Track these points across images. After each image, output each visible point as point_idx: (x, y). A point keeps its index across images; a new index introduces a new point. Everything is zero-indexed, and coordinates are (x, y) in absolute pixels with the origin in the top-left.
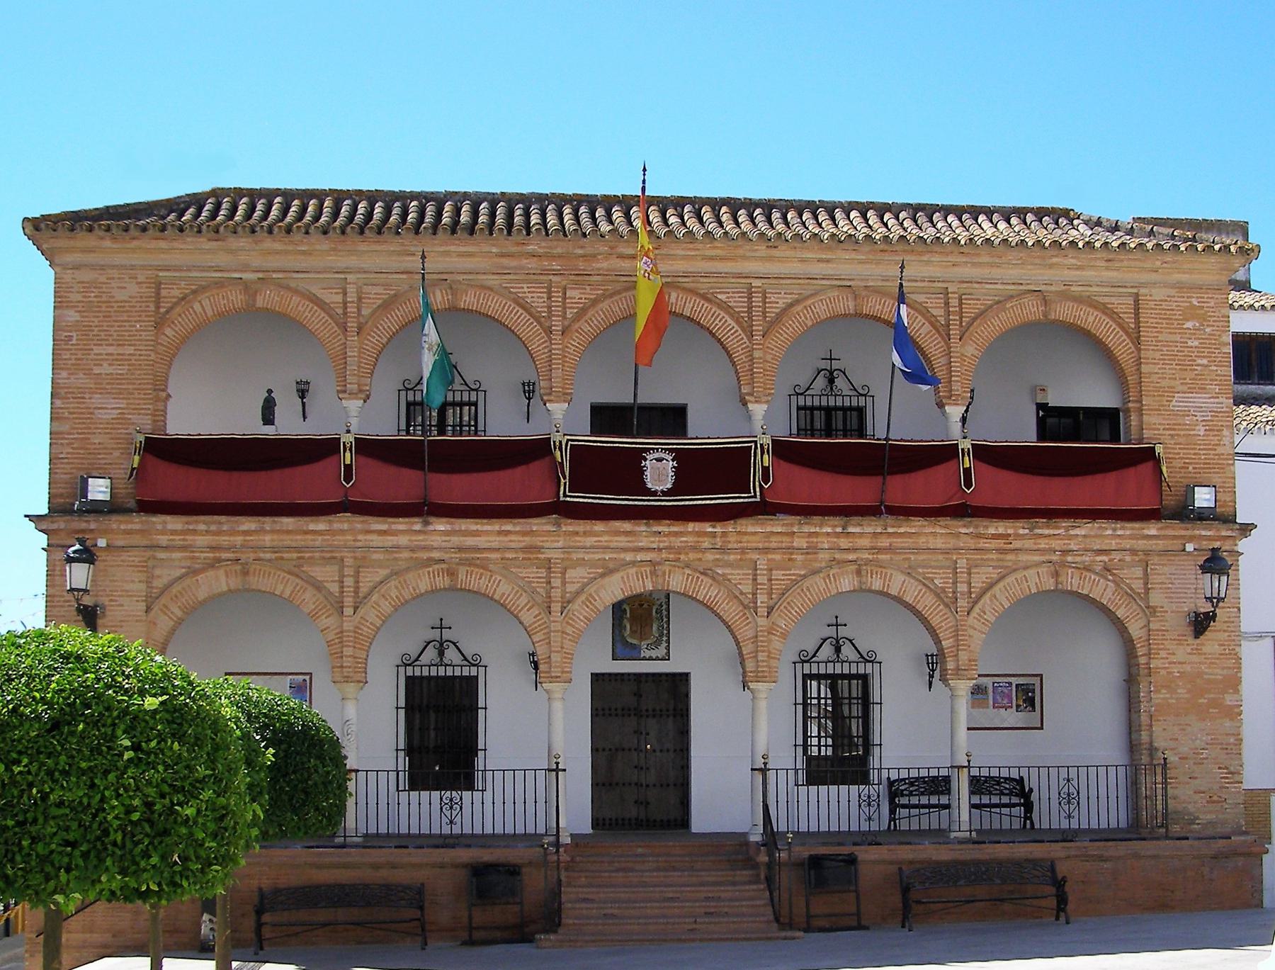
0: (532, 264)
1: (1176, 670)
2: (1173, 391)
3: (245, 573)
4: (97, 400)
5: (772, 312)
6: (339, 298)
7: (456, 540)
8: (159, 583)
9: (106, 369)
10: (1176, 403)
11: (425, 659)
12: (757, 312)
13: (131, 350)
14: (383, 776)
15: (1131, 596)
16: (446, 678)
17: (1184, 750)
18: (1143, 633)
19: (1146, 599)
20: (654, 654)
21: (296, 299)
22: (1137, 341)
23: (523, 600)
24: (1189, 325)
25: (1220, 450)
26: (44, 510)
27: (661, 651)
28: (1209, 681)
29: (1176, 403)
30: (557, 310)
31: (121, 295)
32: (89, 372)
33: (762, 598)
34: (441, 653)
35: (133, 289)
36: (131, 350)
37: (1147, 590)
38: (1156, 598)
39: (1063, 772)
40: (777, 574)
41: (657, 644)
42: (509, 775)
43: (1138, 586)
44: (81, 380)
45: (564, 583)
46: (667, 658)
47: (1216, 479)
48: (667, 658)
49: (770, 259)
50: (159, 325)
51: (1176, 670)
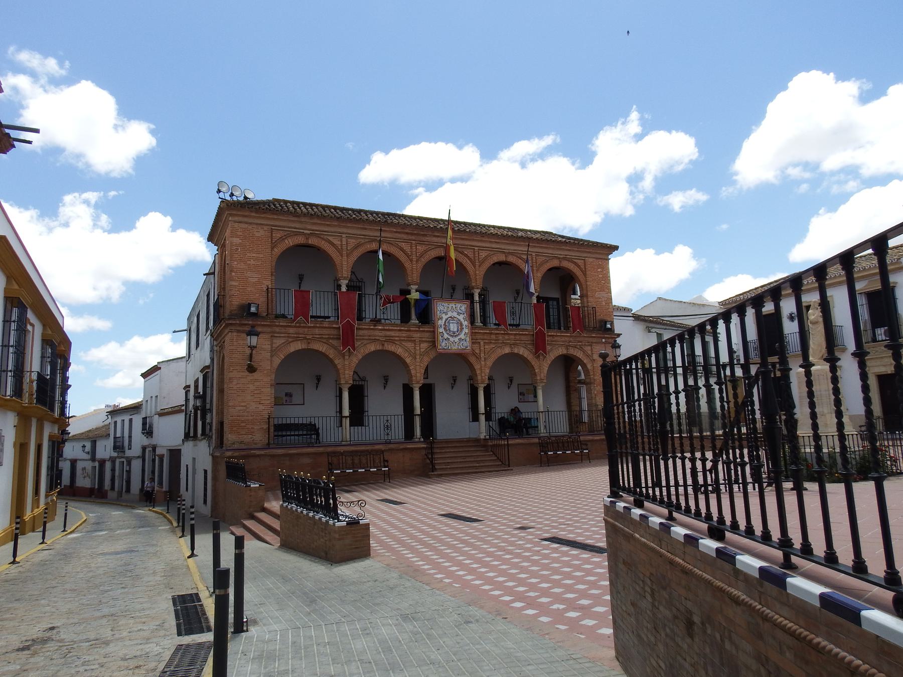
0: (405, 236)
4: (249, 274)
9: (252, 262)
10: (597, 295)
15: (588, 356)
29: (597, 295)
31: (257, 234)
33: (482, 355)
40: (486, 347)
43: (589, 352)
49: (481, 241)
50: (272, 249)
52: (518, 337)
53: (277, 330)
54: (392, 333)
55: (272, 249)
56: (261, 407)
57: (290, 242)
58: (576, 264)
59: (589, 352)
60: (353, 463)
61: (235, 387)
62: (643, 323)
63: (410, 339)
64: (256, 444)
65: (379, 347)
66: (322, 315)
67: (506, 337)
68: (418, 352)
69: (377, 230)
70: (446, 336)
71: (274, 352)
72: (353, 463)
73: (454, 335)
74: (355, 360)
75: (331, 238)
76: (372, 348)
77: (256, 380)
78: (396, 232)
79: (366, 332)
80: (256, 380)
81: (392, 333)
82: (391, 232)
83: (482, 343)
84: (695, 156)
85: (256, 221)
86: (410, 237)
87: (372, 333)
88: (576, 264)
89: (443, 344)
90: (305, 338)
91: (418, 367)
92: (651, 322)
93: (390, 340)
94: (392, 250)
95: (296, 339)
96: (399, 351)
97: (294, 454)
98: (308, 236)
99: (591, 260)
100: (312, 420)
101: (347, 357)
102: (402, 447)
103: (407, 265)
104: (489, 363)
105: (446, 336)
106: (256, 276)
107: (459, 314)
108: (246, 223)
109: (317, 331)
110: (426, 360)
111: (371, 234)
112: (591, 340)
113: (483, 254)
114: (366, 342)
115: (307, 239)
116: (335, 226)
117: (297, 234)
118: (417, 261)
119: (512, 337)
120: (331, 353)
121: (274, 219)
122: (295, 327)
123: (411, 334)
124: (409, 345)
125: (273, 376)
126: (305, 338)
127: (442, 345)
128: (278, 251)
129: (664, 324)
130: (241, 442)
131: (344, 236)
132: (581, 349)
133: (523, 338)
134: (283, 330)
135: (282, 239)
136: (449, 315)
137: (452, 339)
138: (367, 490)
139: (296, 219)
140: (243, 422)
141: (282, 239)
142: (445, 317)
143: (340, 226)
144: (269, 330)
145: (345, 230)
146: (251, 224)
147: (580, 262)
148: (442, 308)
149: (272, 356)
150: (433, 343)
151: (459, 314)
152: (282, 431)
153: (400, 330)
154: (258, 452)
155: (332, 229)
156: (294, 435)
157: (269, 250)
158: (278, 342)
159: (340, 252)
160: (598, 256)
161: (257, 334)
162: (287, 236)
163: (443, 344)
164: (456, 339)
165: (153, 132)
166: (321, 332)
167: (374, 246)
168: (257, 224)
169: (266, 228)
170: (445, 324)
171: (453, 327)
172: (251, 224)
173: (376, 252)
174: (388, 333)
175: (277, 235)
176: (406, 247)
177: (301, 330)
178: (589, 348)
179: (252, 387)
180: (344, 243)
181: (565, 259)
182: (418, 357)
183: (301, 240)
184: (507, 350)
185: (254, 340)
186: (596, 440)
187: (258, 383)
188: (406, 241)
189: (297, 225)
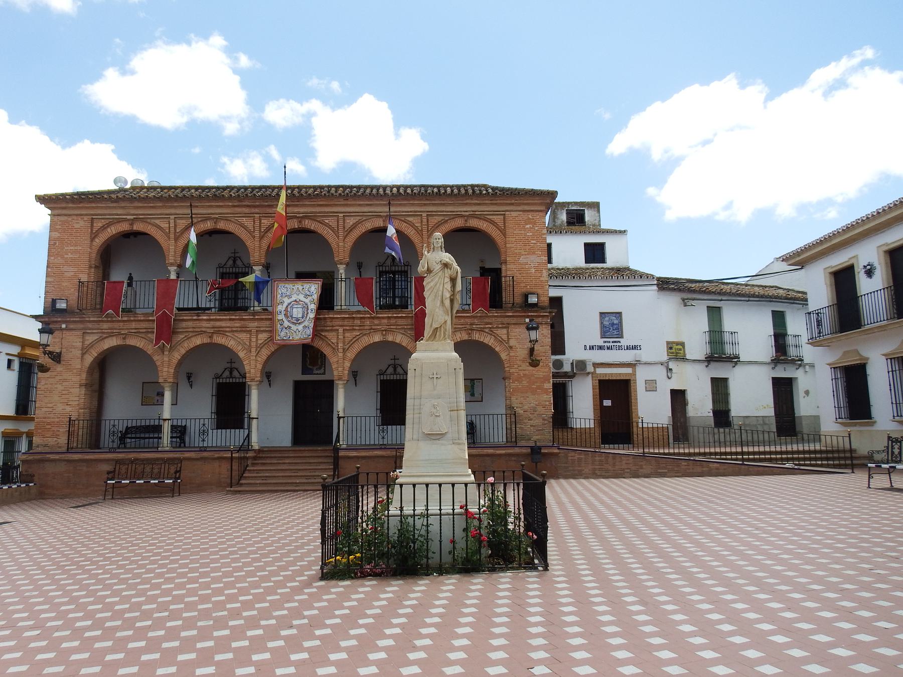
0: (247, 210)
1: (521, 373)
2: (520, 254)
3: (124, 339)
4: (66, 268)
5: (348, 226)
6: (167, 225)
7: (212, 324)
8: (87, 343)
9: (70, 255)
10: (522, 260)
11: (225, 375)
12: (341, 227)
13: (80, 248)
14: (500, 416)
15: (501, 342)
16: (236, 383)
17: (526, 407)
18: (507, 358)
19: (508, 343)
20: (318, 372)
21: (150, 226)
22: (505, 235)
23: (240, 348)
24: (528, 226)
25: (542, 279)
26: (40, 312)
27: (322, 371)
28: (537, 378)
29: (522, 260)
30: (257, 229)
31: (77, 226)
32: (63, 258)
33: (340, 345)
34: (231, 373)
35: (82, 223)
36: (80, 248)
37: (508, 339)
38: (512, 342)
39: (112, 422)
40: (347, 335)
41: (320, 368)
42: (354, 419)
43: (505, 337)
44: (59, 260)
45: (257, 340)
46: (324, 374)
47: (540, 291)
48: (324, 374)
49: (346, 205)
50: (92, 240)
51: (521, 373)
52: (393, 321)
53: (90, 325)
54: (223, 324)
55: (92, 240)
56: (68, 409)
57: (113, 230)
58: (492, 222)
59: (505, 337)
60: (152, 472)
61: (43, 388)
62: (674, 293)
63: (244, 330)
64: (60, 447)
65: (206, 340)
66: (186, 306)
67: (376, 322)
68: (253, 344)
69: (384, 205)
70: (286, 324)
71: (85, 351)
72: (152, 472)
73: (297, 322)
74: (177, 356)
75: (157, 222)
76: (198, 341)
77: (65, 380)
78: (235, 206)
79: (190, 324)
80: (65, 380)
81: (223, 324)
82: (228, 206)
83: (341, 330)
84: (218, 40)
85: (72, 212)
86: (253, 210)
87: (198, 324)
88: (492, 222)
89: (282, 334)
90: (120, 334)
91: (253, 363)
92: (690, 291)
93: (220, 331)
94: (404, 227)
95: (111, 335)
96: (231, 344)
97: (91, 460)
98: (132, 222)
99: (514, 214)
100: (474, 417)
101: (166, 353)
102: (216, 456)
103: (249, 243)
104: (351, 355)
105: (286, 324)
106: (72, 269)
107: (306, 296)
108: (66, 215)
109: (134, 325)
110: (265, 353)
111: (205, 211)
112: (506, 320)
113: (350, 222)
114: (191, 334)
115: (132, 224)
116: (160, 207)
117: (119, 221)
118: (261, 238)
119: (385, 321)
120: (150, 349)
121: (93, 208)
122: (108, 321)
123: (246, 323)
124: (244, 336)
125: (84, 376)
126: (120, 334)
127: (282, 335)
128: (99, 241)
129: (725, 294)
130: (46, 446)
131: (172, 217)
132: (491, 332)
133: (400, 322)
134: (97, 326)
135: (104, 228)
136: (293, 298)
137: (294, 327)
138: (24, 510)
139: (115, 205)
140: (49, 424)
141: (104, 228)
142: (287, 301)
143: (166, 207)
144: (80, 326)
145: (173, 211)
146: (70, 215)
147: (498, 219)
148: (284, 291)
149: (83, 354)
150: (272, 331)
151: (306, 296)
152: (149, 432)
153: (230, 319)
154: (52, 457)
155: (159, 211)
156: (149, 438)
157: (88, 242)
158: (90, 339)
159: (168, 235)
160: (526, 208)
161: (536, 329)
162: (109, 225)
163: (282, 334)
164: (300, 327)
165: (424, 138)
166: (138, 326)
167: (379, 223)
168: (77, 215)
169: (86, 218)
170: (286, 310)
171: (297, 312)
172: (70, 215)
173: (384, 230)
174: (218, 324)
175: (98, 225)
176: (248, 222)
177: (116, 325)
178: (505, 331)
179: (60, 387)
180: (172, 225)
181: (473, 216)
182: (253, 350)
183: (124, 227)
184: (377, 338)
185: (533, 335)
186: (500, 455)
187: (67, 383)
188: (246, 215)
189: (120, 211)
